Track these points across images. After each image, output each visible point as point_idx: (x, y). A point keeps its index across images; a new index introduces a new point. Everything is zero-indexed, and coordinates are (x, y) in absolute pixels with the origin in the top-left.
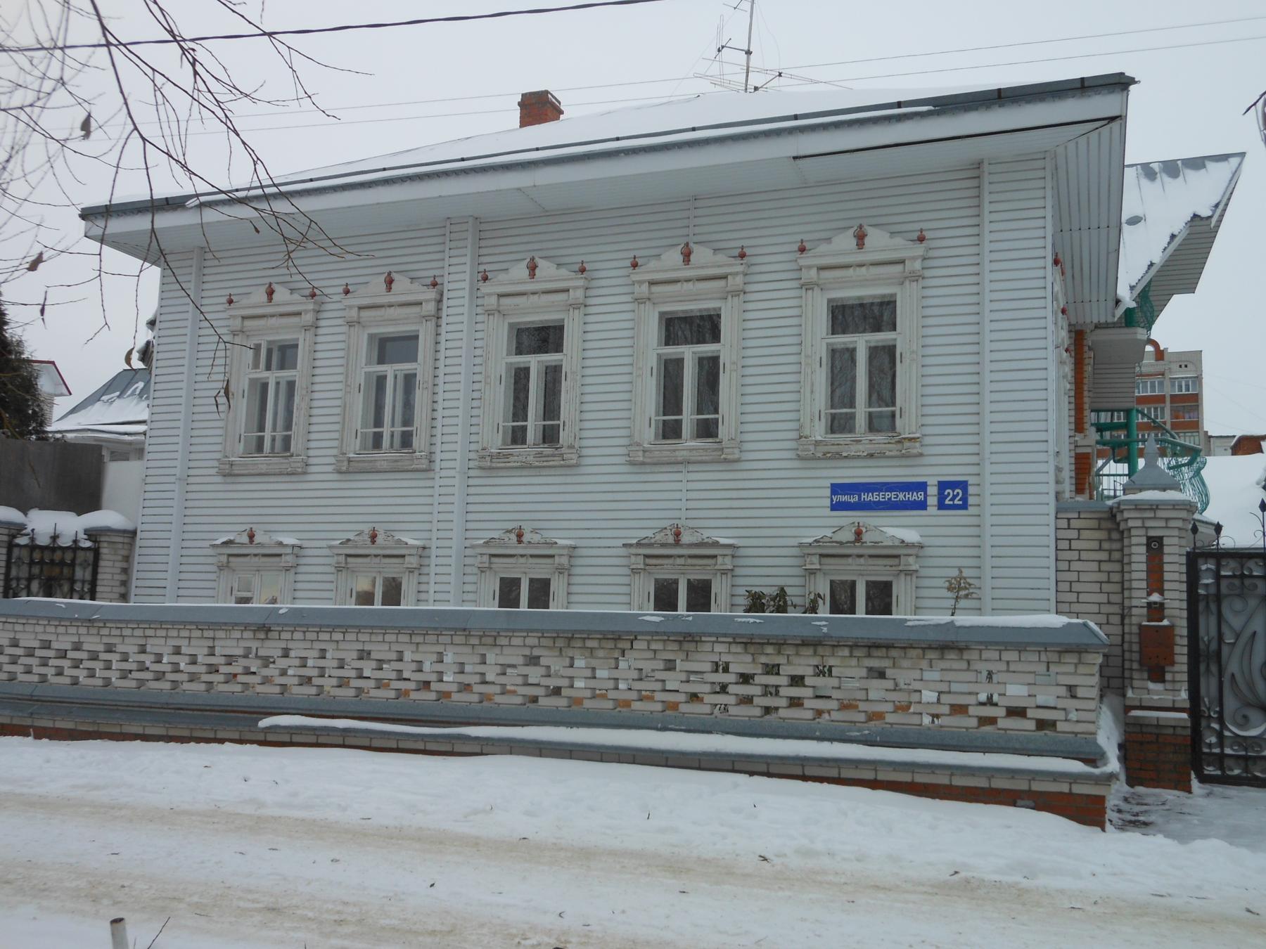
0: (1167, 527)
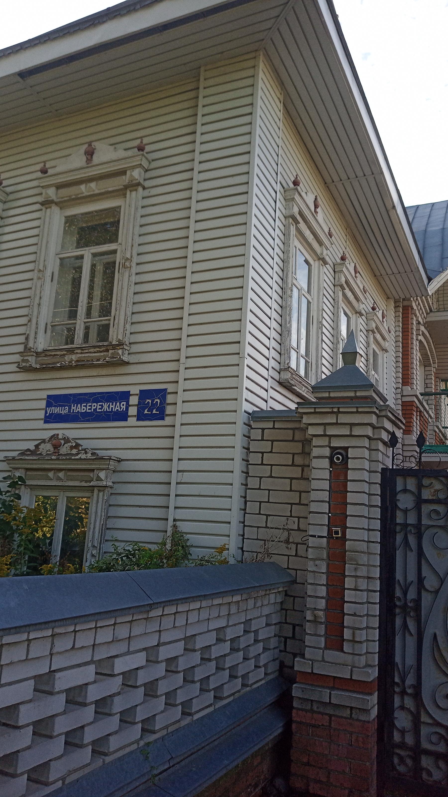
0: (351, 436)
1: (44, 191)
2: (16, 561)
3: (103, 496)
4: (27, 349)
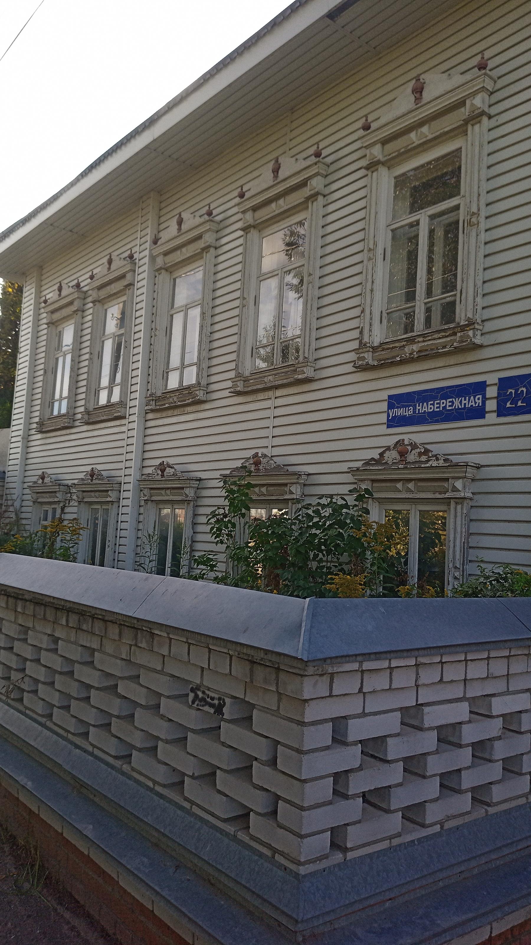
1: (368, 152)
2: (370, 581)
3: (462, 509)
4: (362, 345)
